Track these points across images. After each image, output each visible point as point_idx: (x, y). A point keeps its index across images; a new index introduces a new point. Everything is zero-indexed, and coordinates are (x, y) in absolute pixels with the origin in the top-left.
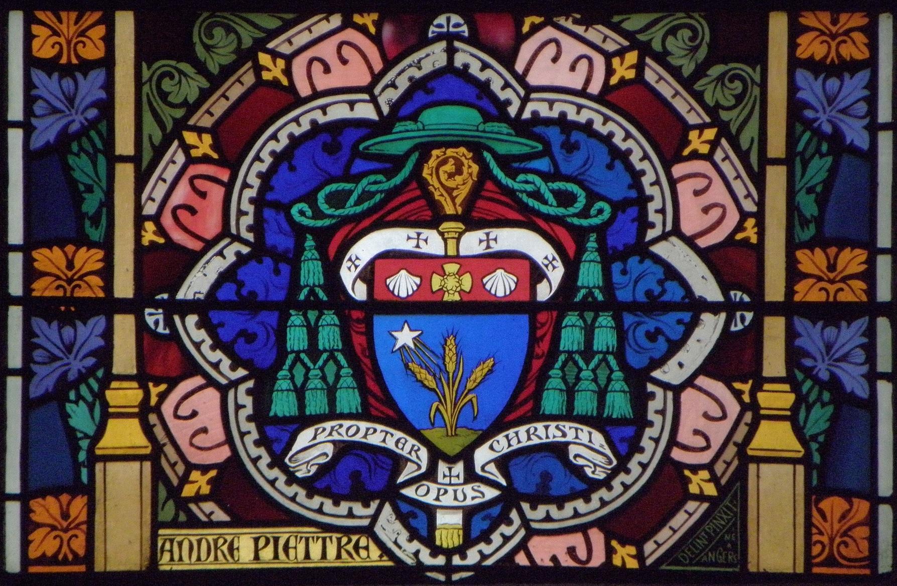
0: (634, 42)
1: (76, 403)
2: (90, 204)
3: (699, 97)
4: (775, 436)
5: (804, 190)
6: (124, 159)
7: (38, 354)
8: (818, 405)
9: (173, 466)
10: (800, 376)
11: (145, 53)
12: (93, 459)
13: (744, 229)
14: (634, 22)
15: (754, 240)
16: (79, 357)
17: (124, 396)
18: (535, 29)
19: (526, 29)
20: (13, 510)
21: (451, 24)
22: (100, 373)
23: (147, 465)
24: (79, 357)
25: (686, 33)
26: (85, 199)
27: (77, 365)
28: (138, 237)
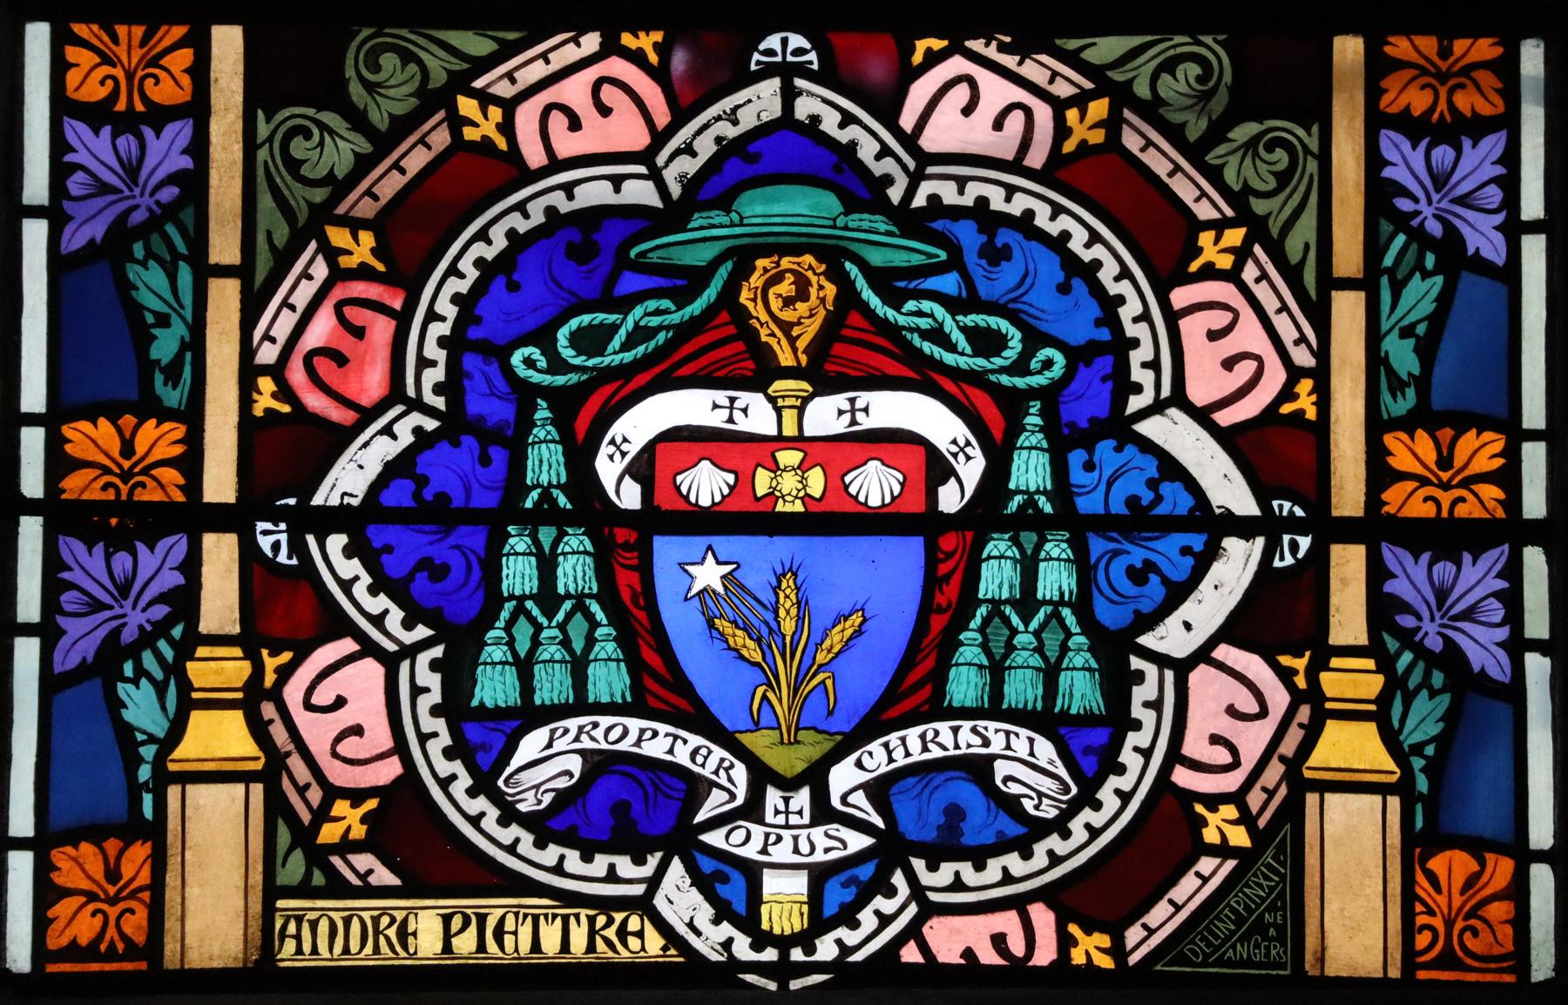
0: (1102, 80)
1: (135, 682)
2: (165, 346)
3: (1214, 175)
4: (1350, 746)
5: (1396, 331)
6: (224, 271)
7: (76, 184)
8: (1425, 693)
9: (302, 790)
10: (1392, 644)
11: (257, 97)
12: (163, 778)
13: (1295, 397)
14: (1105, 49)
15: (1311, 414)
16: (142, 603)
17: (218, 670)
18: (933, 59)
19: (917, 58)
20: (21, 865)
21: (790, 49)
22: (177, 632)
23: (257, 790)
24: (142, 603)
25: (1194, 70)
26: (155, 337)
27: (136, 620)
28: (246, 402)
